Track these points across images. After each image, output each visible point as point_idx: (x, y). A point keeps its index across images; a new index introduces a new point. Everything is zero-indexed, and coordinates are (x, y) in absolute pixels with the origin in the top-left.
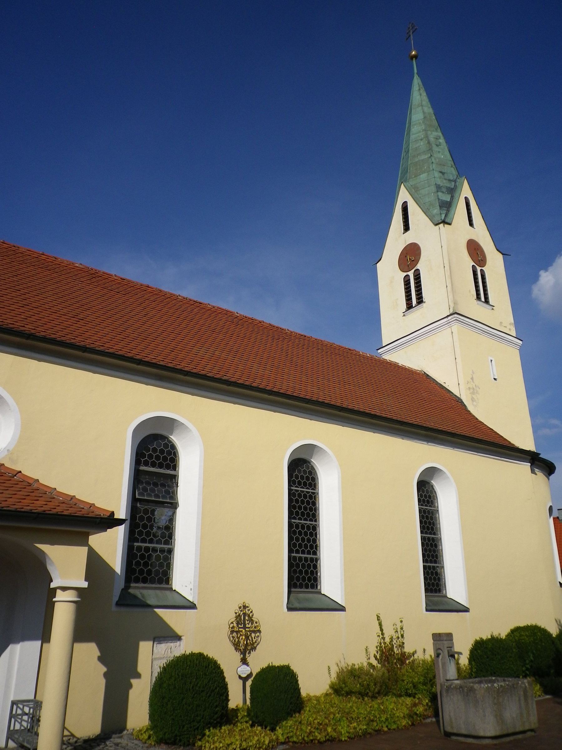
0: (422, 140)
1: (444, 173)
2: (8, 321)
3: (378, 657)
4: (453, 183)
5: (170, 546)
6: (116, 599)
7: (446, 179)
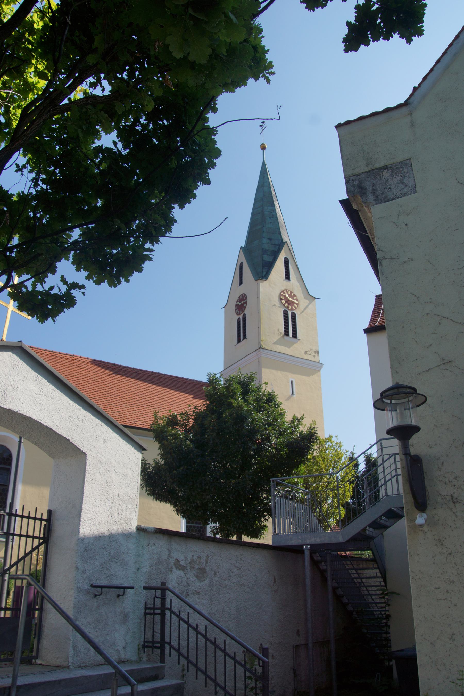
0: (259, 213)
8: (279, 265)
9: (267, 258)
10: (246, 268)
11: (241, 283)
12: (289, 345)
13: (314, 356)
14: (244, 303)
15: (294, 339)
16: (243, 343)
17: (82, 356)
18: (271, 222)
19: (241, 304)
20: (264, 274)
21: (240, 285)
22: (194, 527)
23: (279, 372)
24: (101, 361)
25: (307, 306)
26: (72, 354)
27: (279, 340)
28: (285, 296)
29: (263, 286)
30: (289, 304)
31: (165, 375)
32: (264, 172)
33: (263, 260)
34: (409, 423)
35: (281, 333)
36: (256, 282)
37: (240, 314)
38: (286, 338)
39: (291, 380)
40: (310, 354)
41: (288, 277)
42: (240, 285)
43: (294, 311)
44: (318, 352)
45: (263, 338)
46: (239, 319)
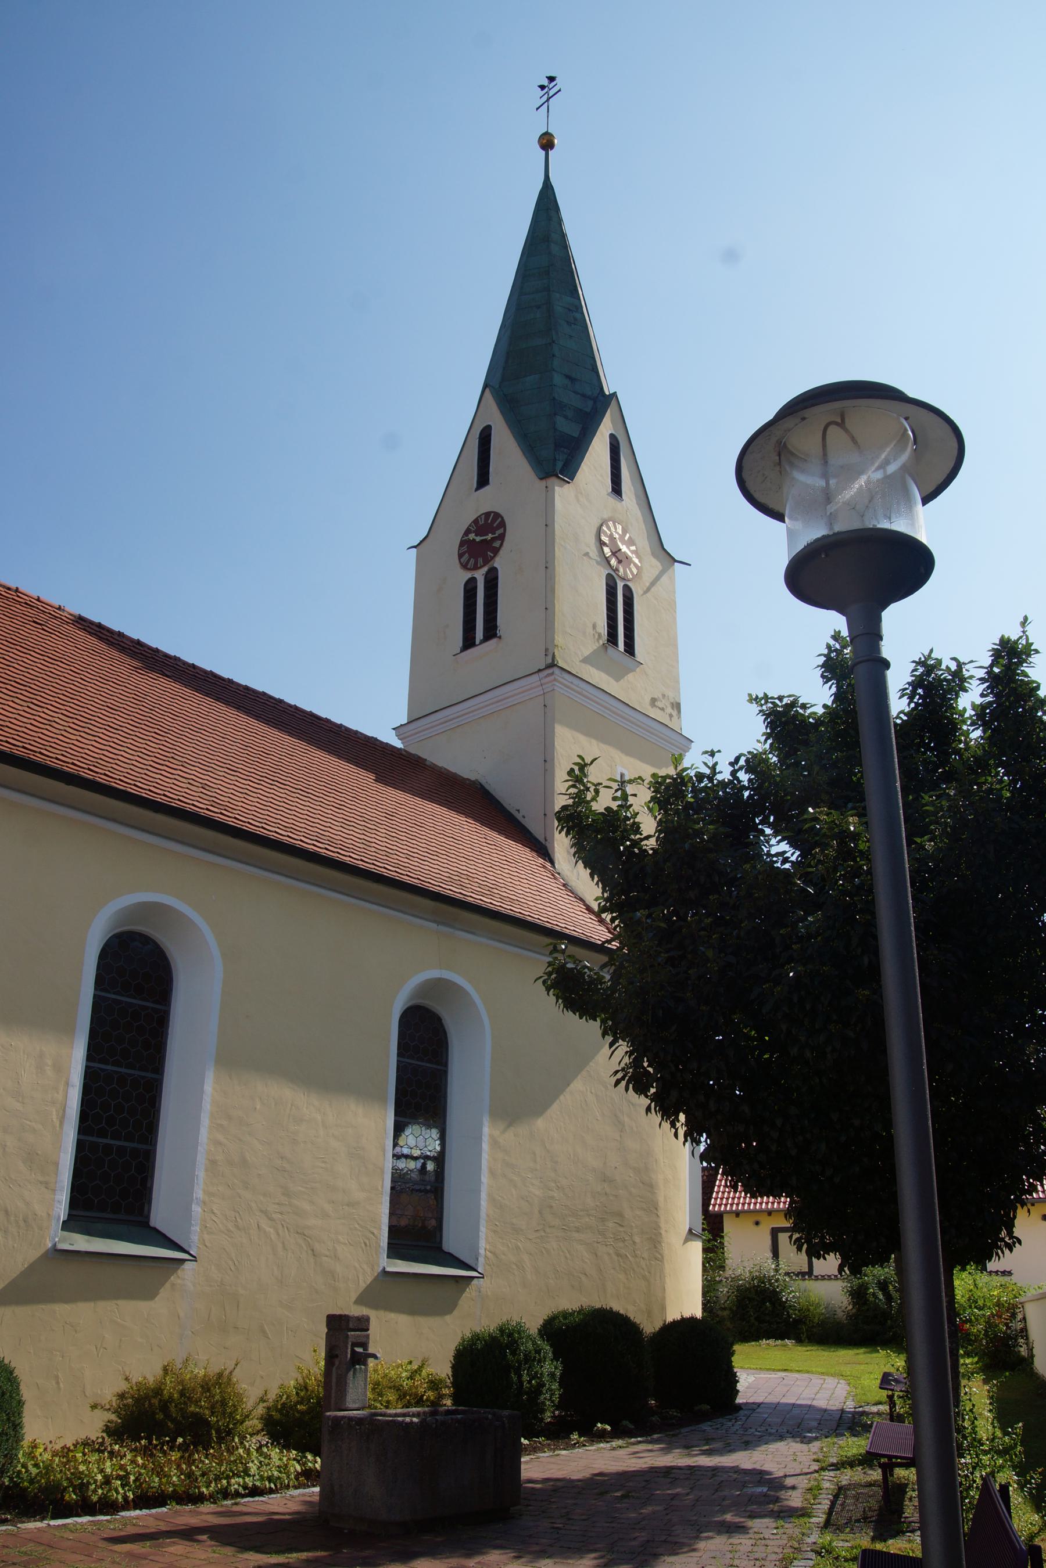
0: (538, 307)
4: (590, 403)
8: (598, 451)
9: (568, 427)
11: (483, 480)
13: (671, 716)
14: (493, 539)
15: (627, 659)
16: (483, 650)
17: (42, 598)
18: (571, 337)
19: (481, 542)
20: (559, 465)
21: (476, 490)
23: (594, 742)
24: (99, 625)
25: (657, 579)
26: (13, 586)
27: (594, 652)
28: (612, 538)
29: (563, 495)
30: (620, 562)
31: (281, 701)
32: (547, 205)
33: (555, 430)
35: (600, 635)
36: (543, 483)
37: (476, 568)
38: (611, 650)
39: (620, 770)
41: (617, 489)
42: (476, 490)
43: (629, 583)
44: (677, 706)
45: (559, 639)
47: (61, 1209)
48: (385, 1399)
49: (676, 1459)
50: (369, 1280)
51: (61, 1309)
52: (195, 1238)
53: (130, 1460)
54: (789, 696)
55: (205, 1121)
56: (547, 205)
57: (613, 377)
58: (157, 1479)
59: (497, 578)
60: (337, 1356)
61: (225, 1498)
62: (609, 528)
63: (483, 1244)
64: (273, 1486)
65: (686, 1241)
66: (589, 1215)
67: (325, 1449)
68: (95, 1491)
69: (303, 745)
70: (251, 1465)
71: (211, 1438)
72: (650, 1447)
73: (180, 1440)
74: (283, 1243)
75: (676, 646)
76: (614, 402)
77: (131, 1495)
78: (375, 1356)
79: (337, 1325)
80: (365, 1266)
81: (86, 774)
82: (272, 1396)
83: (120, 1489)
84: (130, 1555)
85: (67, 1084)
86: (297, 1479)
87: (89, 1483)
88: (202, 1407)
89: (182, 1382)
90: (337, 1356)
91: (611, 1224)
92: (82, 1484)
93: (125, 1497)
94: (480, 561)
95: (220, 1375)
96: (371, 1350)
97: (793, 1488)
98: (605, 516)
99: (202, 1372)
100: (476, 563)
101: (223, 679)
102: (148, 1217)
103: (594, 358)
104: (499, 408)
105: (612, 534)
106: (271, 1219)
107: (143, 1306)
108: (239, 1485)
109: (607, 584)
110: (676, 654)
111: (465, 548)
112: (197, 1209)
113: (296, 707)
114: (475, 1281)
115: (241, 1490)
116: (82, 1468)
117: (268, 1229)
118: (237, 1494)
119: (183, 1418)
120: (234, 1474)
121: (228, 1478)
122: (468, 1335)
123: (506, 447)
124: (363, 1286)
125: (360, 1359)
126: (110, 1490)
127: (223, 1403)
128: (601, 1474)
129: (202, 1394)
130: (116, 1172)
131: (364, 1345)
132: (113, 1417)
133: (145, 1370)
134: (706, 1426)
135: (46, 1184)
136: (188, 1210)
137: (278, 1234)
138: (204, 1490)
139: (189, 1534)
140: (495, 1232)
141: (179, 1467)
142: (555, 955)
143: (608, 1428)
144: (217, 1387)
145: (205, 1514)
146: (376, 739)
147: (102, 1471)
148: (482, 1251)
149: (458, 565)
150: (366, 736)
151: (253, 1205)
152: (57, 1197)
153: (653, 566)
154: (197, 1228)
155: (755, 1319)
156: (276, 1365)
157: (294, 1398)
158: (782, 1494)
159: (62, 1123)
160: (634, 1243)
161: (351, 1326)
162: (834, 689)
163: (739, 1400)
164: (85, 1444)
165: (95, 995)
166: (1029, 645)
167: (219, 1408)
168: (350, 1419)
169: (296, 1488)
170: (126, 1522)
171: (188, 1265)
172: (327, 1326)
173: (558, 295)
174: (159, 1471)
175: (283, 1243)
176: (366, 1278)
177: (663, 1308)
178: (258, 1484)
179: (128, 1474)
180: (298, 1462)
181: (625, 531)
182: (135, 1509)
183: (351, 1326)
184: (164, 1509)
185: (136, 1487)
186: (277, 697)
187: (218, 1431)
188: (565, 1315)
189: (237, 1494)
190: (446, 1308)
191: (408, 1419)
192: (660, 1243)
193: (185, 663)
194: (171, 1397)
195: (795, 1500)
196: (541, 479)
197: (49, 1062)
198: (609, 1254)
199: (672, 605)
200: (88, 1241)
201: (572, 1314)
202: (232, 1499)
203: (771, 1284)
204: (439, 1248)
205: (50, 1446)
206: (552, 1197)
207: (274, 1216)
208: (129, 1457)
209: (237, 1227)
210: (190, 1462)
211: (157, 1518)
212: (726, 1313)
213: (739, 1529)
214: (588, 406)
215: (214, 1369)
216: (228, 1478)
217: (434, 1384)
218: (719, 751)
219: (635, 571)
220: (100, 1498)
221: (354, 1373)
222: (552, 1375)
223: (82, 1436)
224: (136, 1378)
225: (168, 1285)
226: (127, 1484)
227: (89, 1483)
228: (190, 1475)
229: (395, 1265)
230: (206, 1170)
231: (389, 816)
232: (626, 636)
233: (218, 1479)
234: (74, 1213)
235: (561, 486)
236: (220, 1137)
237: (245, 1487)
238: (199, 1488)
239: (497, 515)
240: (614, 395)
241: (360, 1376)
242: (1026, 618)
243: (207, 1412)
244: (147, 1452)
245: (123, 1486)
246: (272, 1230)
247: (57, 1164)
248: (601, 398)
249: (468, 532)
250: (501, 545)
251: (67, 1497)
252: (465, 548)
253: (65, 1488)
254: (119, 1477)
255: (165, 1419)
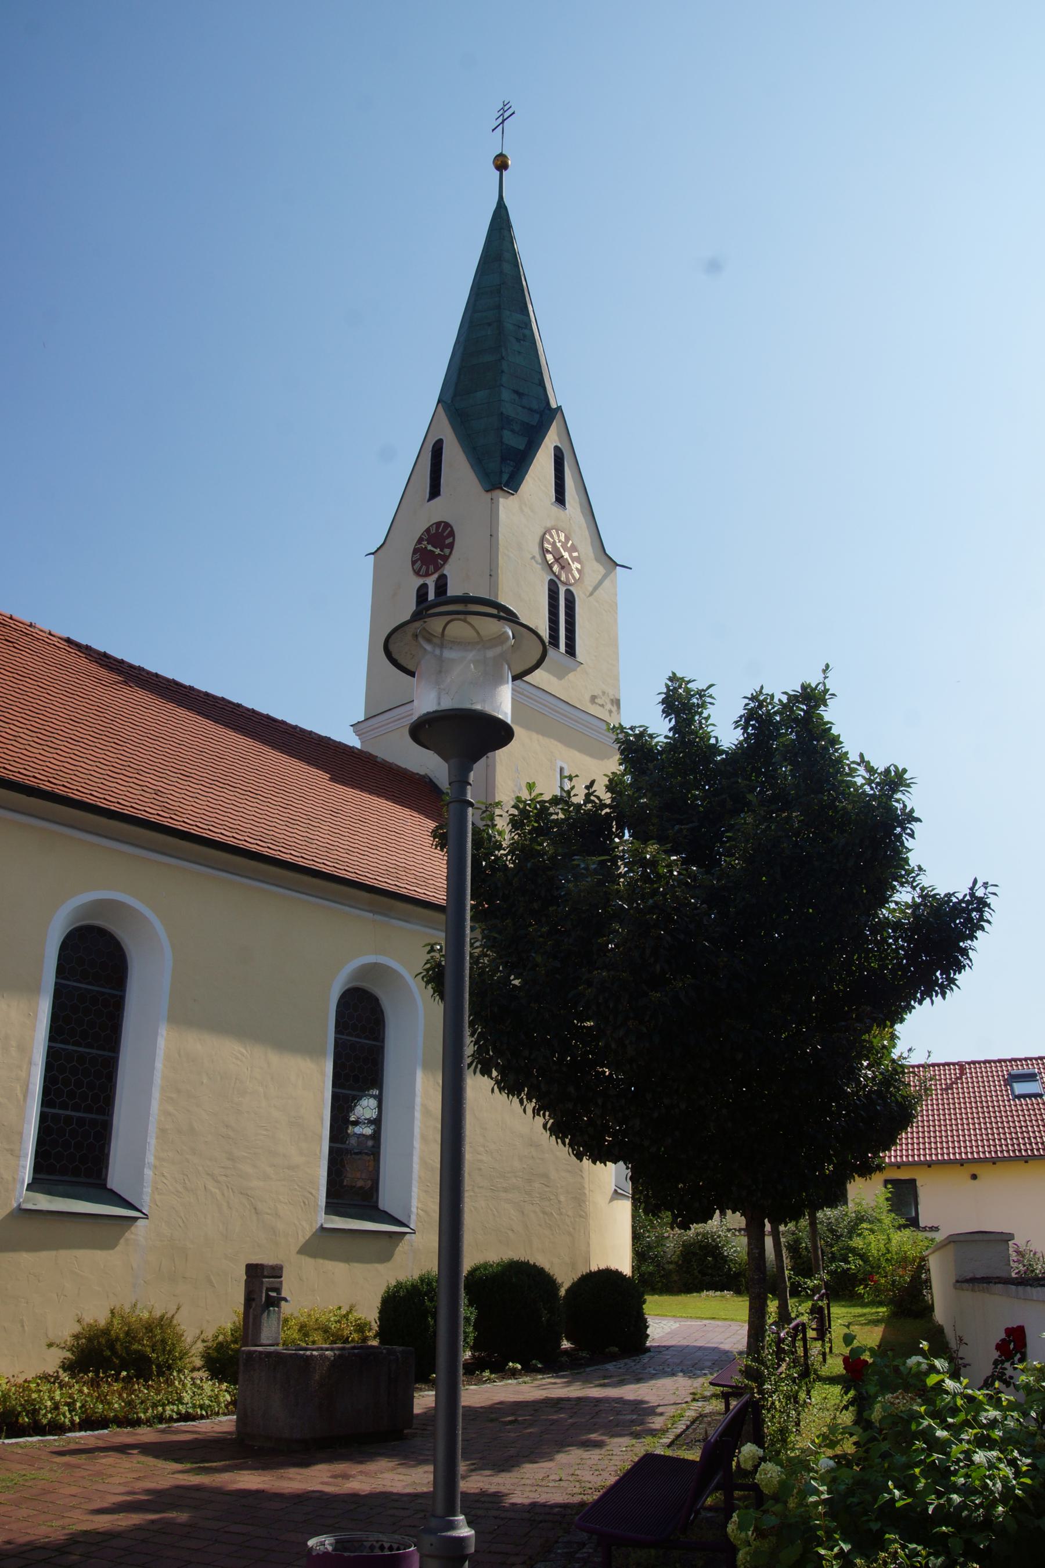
0: (489, 324)
1: (523, 394)
2: (4, 773)
3: (1018, 1356)
4: (537, 417)
5: (106, 1118)
6: (27, 1181)
7: (524, 407)
8: (543, 463)
9: (514, 441)
10: (455, 457)
11: (435, 491)
12: (560, 674)
13: (610, 712)
15: (568, 660)
17: (14, 617)
19: (434, 547)
20: (505, 477)
21: (429, 500)
22: (68, 1120)
23: (535, 736)
25: (601, 582)
28: (554, 544)
29: (507, 506)
30: (563, 568)
31: (239, 706)
32: (501, 224)
33: (502, 442)
34: (358, 1268)
36: (489, 495)
37: (427, 574)
39: (560, 763)
40: (602, 706)
41: (560, 498)
42: (429, 500)
43: (571, 588)
44: (617, 702)
46: (424, 588)
47: (27, 1175)
48: (311, 1339)
49: (575, 1391)
50: (308, 1235)
51: (26, 1258)
52: (147, 1198)
53: (81, 1392)
54: (641, 726)
55: (156, 1094)
56: (501, 224)
57: (562, 387)
58: (101, 1406)
59: (446, 584)
60: (254, 1299)
61: (160, 1422)
62: (552, 536)
63: (415, 1203)
64: (204, 1413)
65: (612, 1200)
66: (516, 1177)
67: (241, 1378)
68: (45, 1415)
69: (258, 745)
70: (184, 1394)
71: (152, 1372)
72: (553, 1380)
73: (124, 1373)
74: (228, 1202)
75: (616, 646)
76: (558, 416)
77: (77, 1419)
78: (285, 1300)
79: (254, 1272)
80: (304, 1224)
81: (46, 787)
82: (209, 1334)
83: (67, 1414)
84: (68, 1465)
85: (30, 1063)
86: (227, 1406)
87: (40, 1408)
88: (144, 1346)
89: (129, 1324)
90: (254, 1299)
91: (537, 1185)
92: (35, 1410)
93: (72, 1421)
94: (432, 568)
95: (162, 1318)
96: (283, 1295)
97: (661, 1414)
98: (549, 525)
99: (146, 1315)
100: (427, 569)
101: (185, 687)
102: (106, 1179)
103: (541, 374)
104: (451, 423)
105: (554, 542)
106: (217, 1182)
107: (99, 1255)
108: (173, 1411)
109: (550, 590)
110: (617, 653)
111: (418, 556)
112: (148, 1173)
113: (253, 711)
114: (407, 1237)
115: (175, 1416)
116: (34, 1396)
117: (214, 1190)
118: (171, 1419)
119: (128, 1354)
120: (169, 1402)
121: (164, 1405)
122: (394, 1283)
123: (457, 463)
124: (302, 1240)
125: (274, 1302)
126: (58, 1414)
127: (164, 1341)
128: (501, 1403)
129: (144, 1334)
130: (76, 1142)
131: (278, 1290)
132: (69, 1355)
133: (97, 1314)
134: (610, 1366)
135: (11, 1152)
136: (141, 1174)
137: (223, 1194)
138: (142, 1415)
139: (123, 1449)
140: (426, 1191)
141: (120, 1395)
142: (433, 954)
143: (519, 1366)
144: (160, 1331)
145: (145, 1434)
146: (329, 738)
147: (52, 1399)
148: (414, 1210)
149: (411, 572)
150: (319, 736)
151: (200, 1168)
152: (21, 1163)
153: (595, 570)
154: (148, 1190)
155: (699, 1272)
156: (208, 1314)
157: (229, 1338)
158: (650, 1419)
159: (25, 1097)
160: (560, 1202)
161: (266, 1273)
162: (673, 722)
163: (648, 1344)
164: (40, 1378)
165: (56, 984)
166: (826, 691)
167: (159, 1347)
168: (261, 1352)
169: (225, 1414)
170: (70, 1439)
171: (140, 1222)
172: (246, 1273)
173: (508, 313)
174: (102, 1399)
175: (228, 1202)
176: (306, 1231)
177: (588, 1261)
178: (190, 1410)
179: (75, 1401)
180: (229, 1392)
181: (567, 539)
182: (80, 1430)
183: (266, 1273)
184: (106, 1431)
185: (82, 1413)
186: (235, 701)
187: (159, 1366)
188: (485, 1266)
189: (171, 1419)
190: (386, 1257)
191: (308, 1353)
192: (584, 1202)
193: (148, 673)
194: (117, 1338)
195: (657, 1423)
196: (487, 491)
197: (14, 1043)
198: (535, 1212)
199: (613, 607)
200: (50, 1202)
201: (491, 1266)
202: (166, 1423)
203: (714, 1240)
204: (375, 1207)
205: (12, 1380)
206: (481, 1161)
207: (219, 1178)
208: (77, 1387)
209: (186, 1188)
210: (133, 1392)
211: (97, 1438)
212: (671, 1267)
213: (599, 1445)
214: (534, 420)
215: (158, 1314)
216: (164, 1405)
217: (361, 1328)
218: (577, 776)
219: (577, 576)
220: (49, 1421)
221: (268, 1314)
222: (467, 1319)
223: (40, 1372)
224: (88, 1319)
225: (122, 1241)
226: (74, 1410)
227: (40, 1408)
228: (130, 1403)
229: (332, 1222)
230: (157, 1138)
231: (334, 813)
232: (567, 637)
233: (155, 1406)
234: (38, 1176)
235: (507, 498)
236: (170, 1109)
237: (179, 1413)
238: (137, 1413)
239: (447, 525)
240: (559, 408)
241: (274, 1317)
242: (827, 666)
243: (148, 1349)
244: (95, 1384)
245: (70, 1411)
246: (217, 1191)
247: (21, 1134)
248: (547, 411)
249: (420, 540)
250: (451, 553)
251: (20, 1420)
252: (418, 556)
253: (20, 1413)
254: (67, 1404)
255: (117, 1357)
